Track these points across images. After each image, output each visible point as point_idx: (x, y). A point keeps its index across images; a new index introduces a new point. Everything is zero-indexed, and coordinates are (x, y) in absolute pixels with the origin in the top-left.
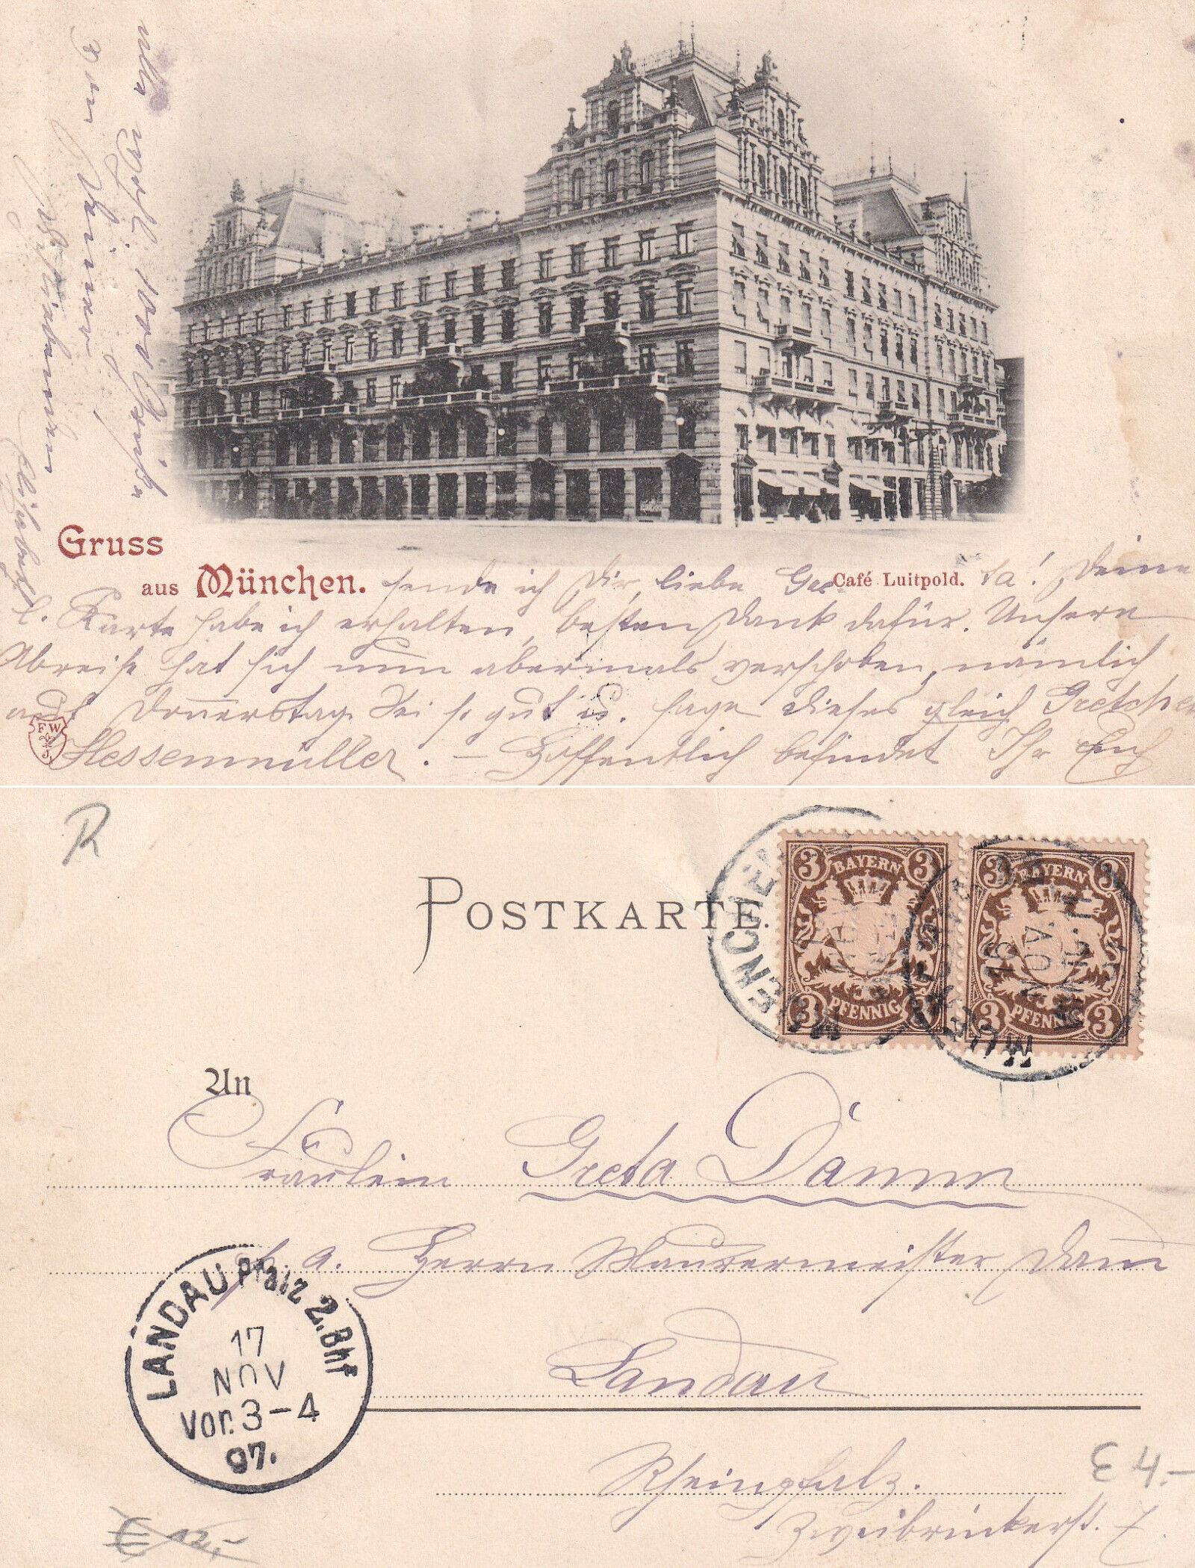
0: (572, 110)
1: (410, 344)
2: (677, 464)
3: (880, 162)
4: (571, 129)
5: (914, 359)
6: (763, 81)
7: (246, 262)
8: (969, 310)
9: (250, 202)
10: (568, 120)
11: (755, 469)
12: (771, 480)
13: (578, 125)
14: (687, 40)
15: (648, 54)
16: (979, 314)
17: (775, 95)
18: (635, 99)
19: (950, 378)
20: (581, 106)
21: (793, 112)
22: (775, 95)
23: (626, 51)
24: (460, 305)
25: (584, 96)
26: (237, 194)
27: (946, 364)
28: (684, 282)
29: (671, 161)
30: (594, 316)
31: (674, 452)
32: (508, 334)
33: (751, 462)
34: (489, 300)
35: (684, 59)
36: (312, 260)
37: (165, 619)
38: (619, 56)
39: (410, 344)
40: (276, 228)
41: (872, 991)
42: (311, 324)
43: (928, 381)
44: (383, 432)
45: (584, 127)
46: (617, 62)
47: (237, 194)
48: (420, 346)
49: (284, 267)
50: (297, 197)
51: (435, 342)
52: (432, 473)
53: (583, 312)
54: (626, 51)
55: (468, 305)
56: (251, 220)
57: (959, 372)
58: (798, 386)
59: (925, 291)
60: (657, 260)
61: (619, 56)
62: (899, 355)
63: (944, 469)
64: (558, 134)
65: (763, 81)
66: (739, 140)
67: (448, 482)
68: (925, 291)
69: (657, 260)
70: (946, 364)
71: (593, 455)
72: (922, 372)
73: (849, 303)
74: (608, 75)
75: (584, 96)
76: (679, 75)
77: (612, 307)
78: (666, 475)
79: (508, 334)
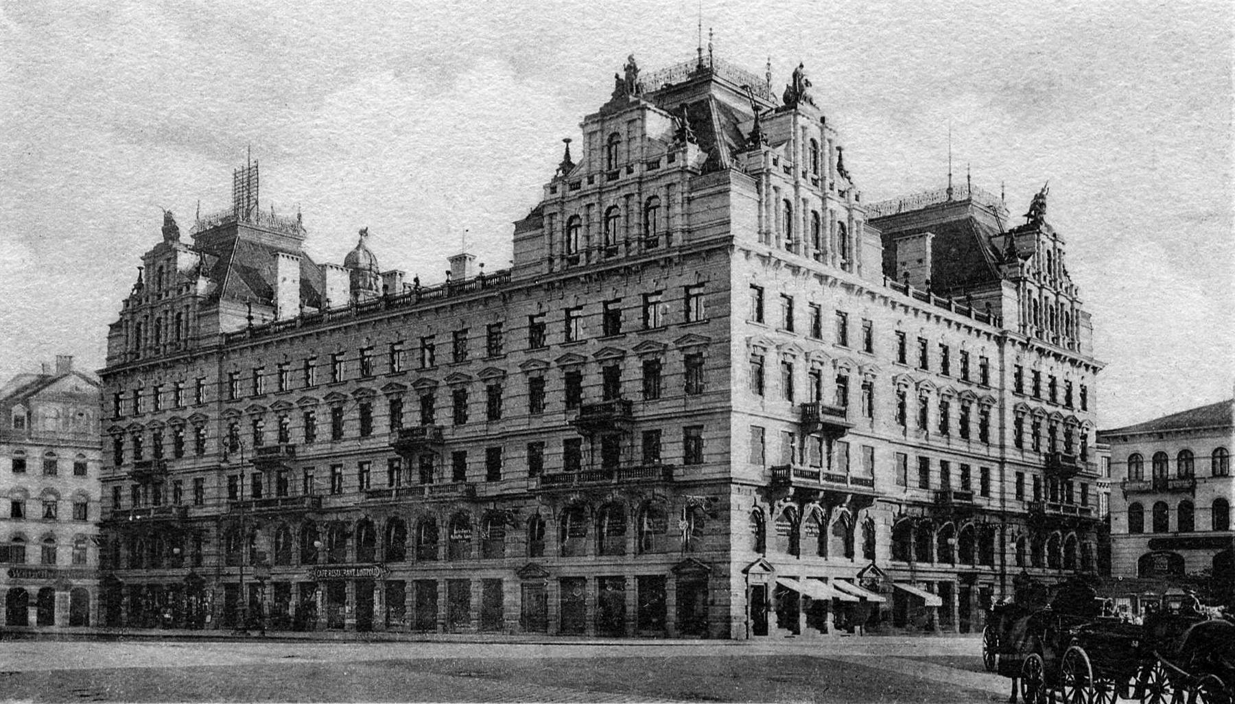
0: (567, 141)
3: (959, 181)
4: (567, 165)
5: (984, 436)
6: (796, 95)
7: (183, 317)
8: (1062, 371)
15: (663, 61)
16: (1077, 377)
20: (578, 137)
21: (830, 141)
23: (632, 69)
24: (440, 376)
26: (170, 229)
27: (1028, 440)
28: (693, 356)
30: (593, 391)
34: (473, 370)
35: (703, 75)
36: (261, 316)
38: (623, 75)
39: (381, 423)
42: (264, 396)
43: (1002, 462)
44: (351, 528)
45: (581, 164)
47: (170, 229)
48: (392, 427)
51: (411, 418)
52: (476, 576)
53: (580, 389)
54: (632, 69)
56: (186, 261)
59: (1001, 352)
61: (623, 75)
62: (965, 433)
64: (549, 172)
65: (796, 95)
68: (1001, 352)
69: (666, 328)
70: (1028, 440)
71: (629, 558)
75: (581, 126)
77: (612, 378)
78: (671, 584)
79: (494, 414)
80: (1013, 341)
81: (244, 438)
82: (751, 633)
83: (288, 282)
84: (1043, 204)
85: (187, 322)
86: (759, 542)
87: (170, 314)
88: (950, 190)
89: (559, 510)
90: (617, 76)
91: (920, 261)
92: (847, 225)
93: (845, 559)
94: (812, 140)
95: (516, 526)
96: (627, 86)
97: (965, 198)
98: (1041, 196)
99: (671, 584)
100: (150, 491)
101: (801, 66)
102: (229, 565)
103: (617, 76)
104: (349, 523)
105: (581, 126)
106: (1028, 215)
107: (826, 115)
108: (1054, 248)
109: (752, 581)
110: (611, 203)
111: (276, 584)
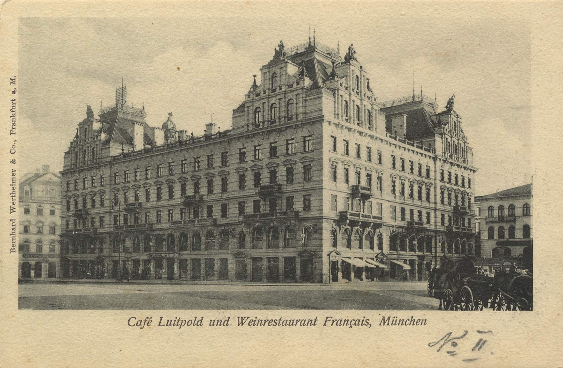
0: (255, 76)
1: (177, 193)
3: (417, 93)
4: (255, 86)
7: (95, 149)
9: (96, 116)
13: (258, 84)
14: (312, 40)
15: (295, 43)
16: (466, 174)
18: (284, 73)
19: (448, 208)
21: (364, 76)
23: (281, 46)
25: (261, 70)
26: (90, 113)
29: (301, 104)
32: (224, 189)
34: (215, 171)
35: (311, 49)
36: (127, 149)
37: (199, 158)
38: (278, 49)
39: (177, 193)
42: (129, 182)
43: (435, 210)
44: (165, 237)
45: (260, 86)
47: (90, 113)
48: (182, 195)
54: (281, 46)
55: (205, 175)
56: (96, 126)
57: (453, 204)
58: (363, 216)
59: (435, 164)
60: (295, 154)
61: (278, 49)
62: (420, 198)
67: (196, 262)
68: (435, 164)
69: (295, 154)
70: (446, 200)
71: (280, 250)
72: (432, 206)
73: (393, 171)
74: (272, 58)
75: (261, 70)
76: (306, 58)
82: (331, 281)
84: (452, 103)
88: (414, 97)
90: (275, 49)
91: (401, 126)
95: (234, 236)
96: (280, 53)
97: (420, 100)
99: (298, 260)
100: (81, 222)
101: (352, 45)
103: (275, 49)
104: (164, 235)
106: (446, 107)
109: (331, 259)
110: (273, 102)
111: (134, 260)
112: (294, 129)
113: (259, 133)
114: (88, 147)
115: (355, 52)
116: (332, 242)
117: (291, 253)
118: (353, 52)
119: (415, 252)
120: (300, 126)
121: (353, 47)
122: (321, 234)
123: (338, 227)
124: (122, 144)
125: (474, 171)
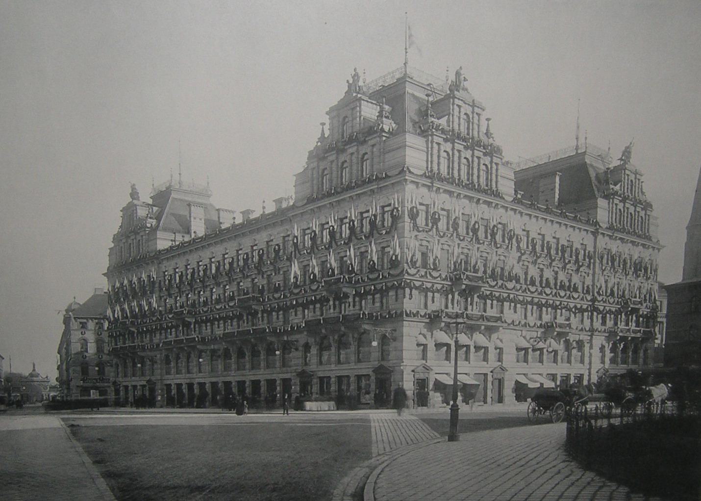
0: (323, 124)
2: (379, 370)
10: (320, 131)
11: (432, 373)
12: (439, 377)
17: (460, 103)
21: (478, 115)
22: (460, 103)
23: (356, 76)
26: (134, 195)
31: (376, 364)
33: (427, 369)
35: (402, 81)
40: (158, 218)
41: (650, 277)
46: (350, 86)
47: (134, 195)
49: (163, 243)
50: (174, 195)
54: (356, 76)
63: (623, 257)
66: (427, 142)
76: (392, 95)
80: (603, 234)
81: (300, 315)
82: (416, 405)
83: (198, 220)
84: (630, 152)
85: (142, 244)
86: (499, 358)
87: (134, 241)
88: (577, 149)
89: (318, 339)
90: (348, 81)
91: (552, 190)
92: (470, 160)
93: (446, 362)
94: (466, 114)
95: (297, 349)
96: (353, 87)
97: (584, 151)
98: (627, 148)
99: (373, 378)
100: (148, 336)
101: (461, 68)
102: (166, 374)
103: (348, 81)
104: (219, 350)
105: (327, 113)
106: (621, 159)
107: (611, 148)
108: (636, 178)
109: (417, 376)
110: (343, 160)
111: (124, 386)
112: (370, 195)
113: (325, 205)
114: (133, 240)
115: (465, 80)
116: (497, 357)
117: (365, 368)
118: (462, 78)
119: (617, 364)
120: (375, 191)
121: (462, 72)
122: (402, 342)
123: (607, 344)
124: (175, 233)
125: (659, 250)
